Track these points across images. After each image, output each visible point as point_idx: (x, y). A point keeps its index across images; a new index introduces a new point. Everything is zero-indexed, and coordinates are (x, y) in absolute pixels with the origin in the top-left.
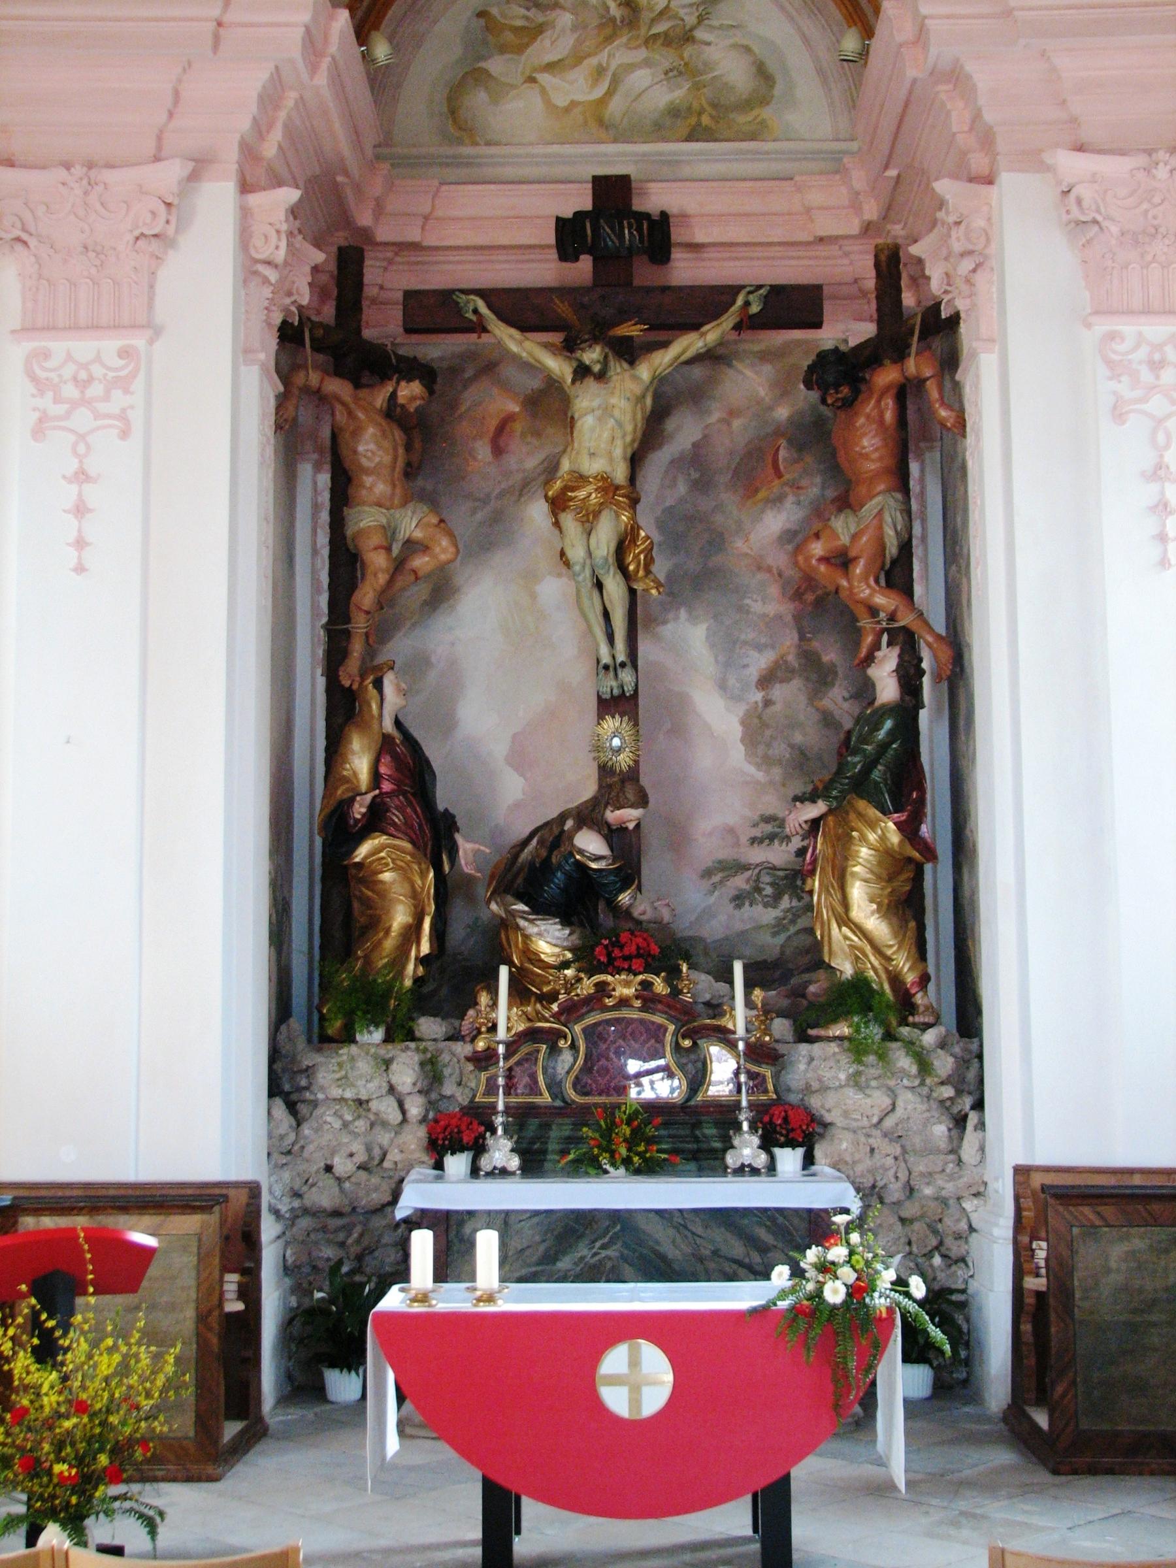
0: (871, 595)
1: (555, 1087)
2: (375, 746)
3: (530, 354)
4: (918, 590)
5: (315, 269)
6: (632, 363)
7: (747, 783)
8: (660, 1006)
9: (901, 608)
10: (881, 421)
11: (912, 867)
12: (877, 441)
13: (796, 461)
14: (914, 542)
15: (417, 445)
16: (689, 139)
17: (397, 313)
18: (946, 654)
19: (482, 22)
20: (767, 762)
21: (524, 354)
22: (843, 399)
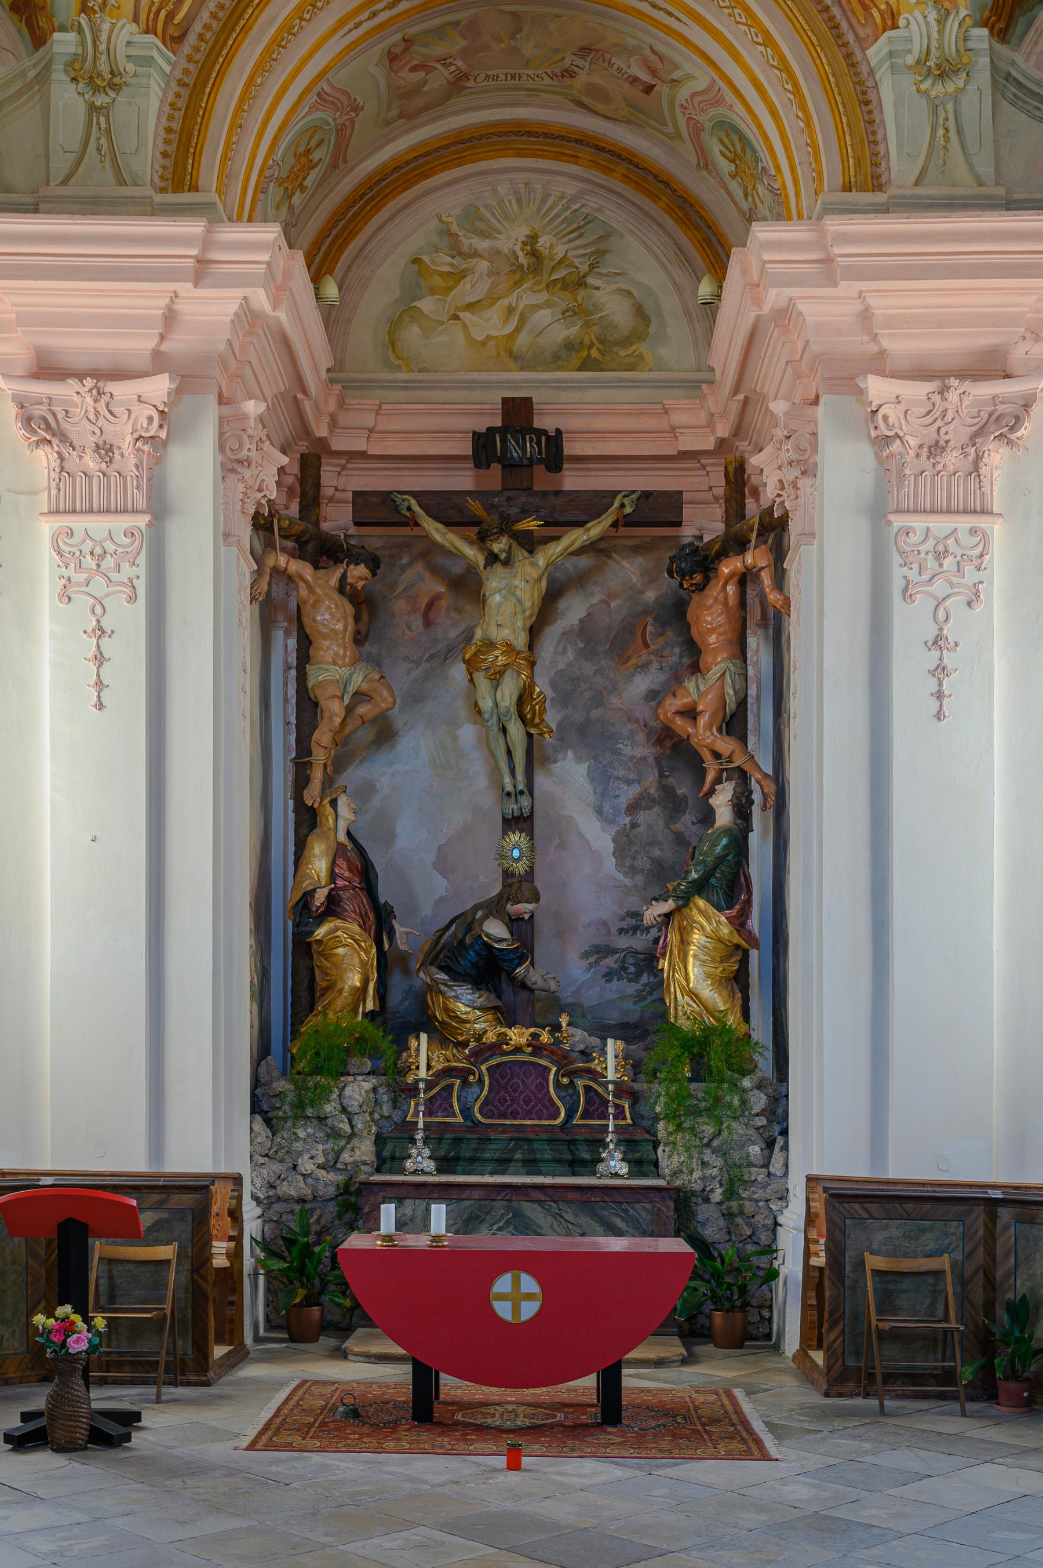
0: (713, 741)
1: (466, 1112)
2: (332, 853)
3: (452, 544)
4: (751, 739)
5: (281, 470)
6: (531, 552)
7: (615, 886)
8: (545, 1052)
9: (737, 751)
10: (726, 603)
11: (740, 952)
12: (721, 619)
13: (660, 635)
14: (750, 700)
15: (365, 617)
16: (580, 369)
17: (348, 511)
18: (771, 788)
19: (416, 267)
20: (633, 871)
21: (447, 544)
22: (696, 584)
